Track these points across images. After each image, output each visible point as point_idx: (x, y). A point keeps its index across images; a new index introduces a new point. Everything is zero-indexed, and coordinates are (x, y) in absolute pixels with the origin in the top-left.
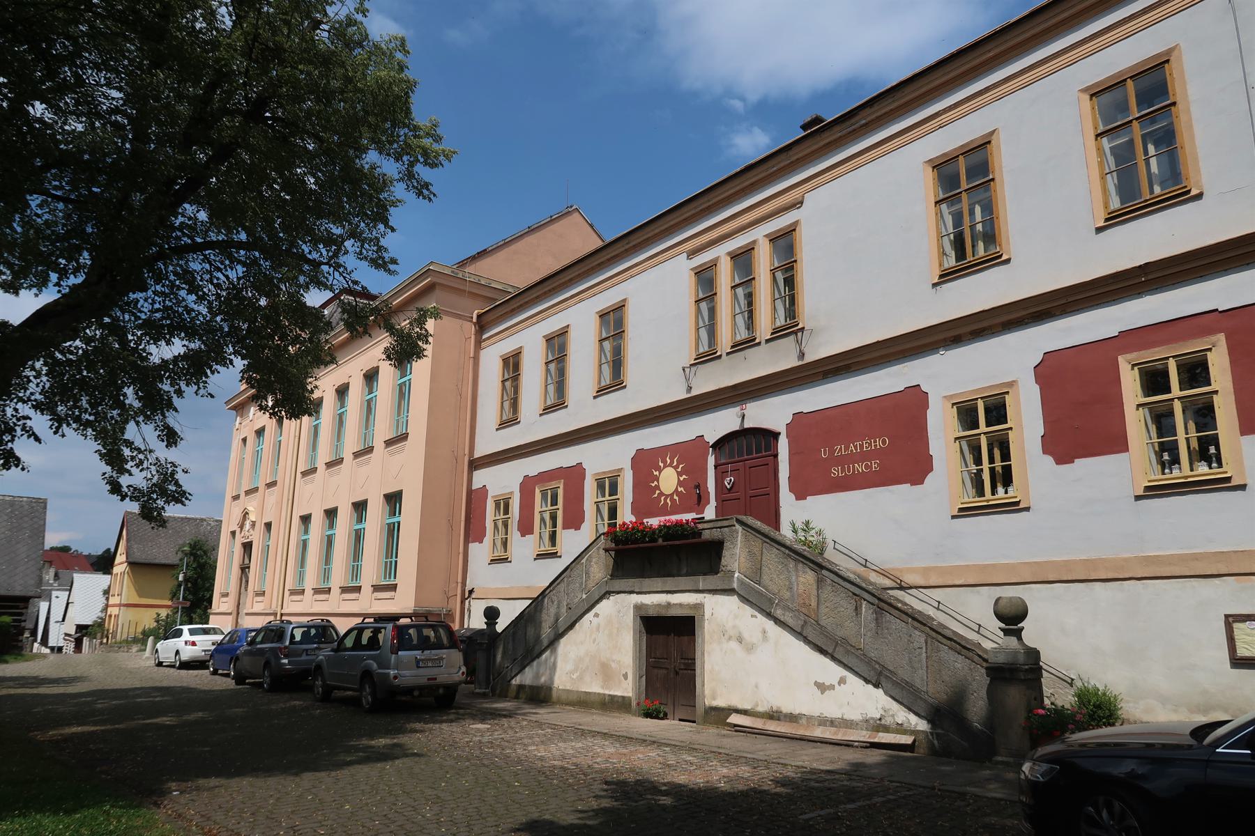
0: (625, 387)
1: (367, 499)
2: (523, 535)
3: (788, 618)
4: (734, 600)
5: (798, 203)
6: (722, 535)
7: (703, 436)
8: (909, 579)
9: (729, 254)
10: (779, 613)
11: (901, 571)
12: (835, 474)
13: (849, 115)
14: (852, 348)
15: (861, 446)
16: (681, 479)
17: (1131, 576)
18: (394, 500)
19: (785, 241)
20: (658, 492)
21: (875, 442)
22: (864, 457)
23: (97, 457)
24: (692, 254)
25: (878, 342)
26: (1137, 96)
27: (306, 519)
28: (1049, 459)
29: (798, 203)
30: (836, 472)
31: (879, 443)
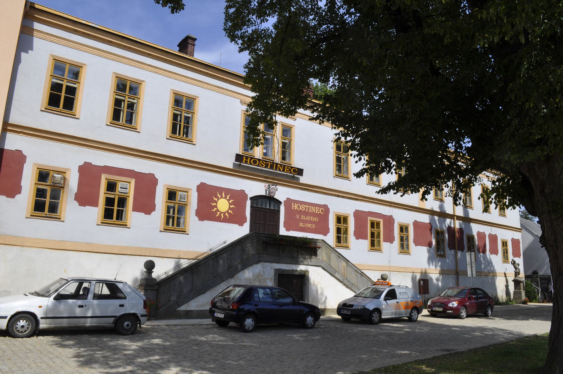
3: (339, 277)
4: (320, 269)
10: (336, 275)
15: (310, 218)
22: (311, 222)
23: (315, 124)
30: (301, 225)
31: (315, 219)
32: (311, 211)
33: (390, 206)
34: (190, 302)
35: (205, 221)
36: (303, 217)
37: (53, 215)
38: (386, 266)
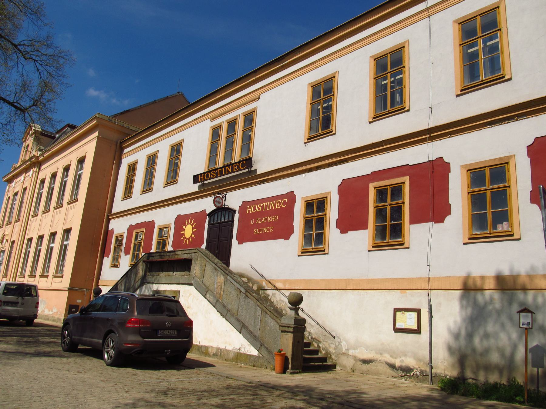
0: (177, 183)
1: (71, 228)
2: (126, 255)
5: (257, 99)
6: (191, 257)
7: (205, 210)
8: (279, 285)
9: (227, 120)
11: (275, 281)
12: (255, 232)
14: (269, 171)
15: (267, 219)
16: (194, 230)
17: (362, 288)
18: (67, 231)
19: (250, 118)
20: (183, 236)
21: (273, 218)
22: (268, 224)
24: (213, 119)
26: (391, 64)
27: (30, 240)
29: (257, 99)
30: (256, 231)
32: (269, 208)
33: (432, 139)
34: (528, 358)
35: (349, 232)
36: (259, 221)
37: (395, 241)
38: (420, 278)
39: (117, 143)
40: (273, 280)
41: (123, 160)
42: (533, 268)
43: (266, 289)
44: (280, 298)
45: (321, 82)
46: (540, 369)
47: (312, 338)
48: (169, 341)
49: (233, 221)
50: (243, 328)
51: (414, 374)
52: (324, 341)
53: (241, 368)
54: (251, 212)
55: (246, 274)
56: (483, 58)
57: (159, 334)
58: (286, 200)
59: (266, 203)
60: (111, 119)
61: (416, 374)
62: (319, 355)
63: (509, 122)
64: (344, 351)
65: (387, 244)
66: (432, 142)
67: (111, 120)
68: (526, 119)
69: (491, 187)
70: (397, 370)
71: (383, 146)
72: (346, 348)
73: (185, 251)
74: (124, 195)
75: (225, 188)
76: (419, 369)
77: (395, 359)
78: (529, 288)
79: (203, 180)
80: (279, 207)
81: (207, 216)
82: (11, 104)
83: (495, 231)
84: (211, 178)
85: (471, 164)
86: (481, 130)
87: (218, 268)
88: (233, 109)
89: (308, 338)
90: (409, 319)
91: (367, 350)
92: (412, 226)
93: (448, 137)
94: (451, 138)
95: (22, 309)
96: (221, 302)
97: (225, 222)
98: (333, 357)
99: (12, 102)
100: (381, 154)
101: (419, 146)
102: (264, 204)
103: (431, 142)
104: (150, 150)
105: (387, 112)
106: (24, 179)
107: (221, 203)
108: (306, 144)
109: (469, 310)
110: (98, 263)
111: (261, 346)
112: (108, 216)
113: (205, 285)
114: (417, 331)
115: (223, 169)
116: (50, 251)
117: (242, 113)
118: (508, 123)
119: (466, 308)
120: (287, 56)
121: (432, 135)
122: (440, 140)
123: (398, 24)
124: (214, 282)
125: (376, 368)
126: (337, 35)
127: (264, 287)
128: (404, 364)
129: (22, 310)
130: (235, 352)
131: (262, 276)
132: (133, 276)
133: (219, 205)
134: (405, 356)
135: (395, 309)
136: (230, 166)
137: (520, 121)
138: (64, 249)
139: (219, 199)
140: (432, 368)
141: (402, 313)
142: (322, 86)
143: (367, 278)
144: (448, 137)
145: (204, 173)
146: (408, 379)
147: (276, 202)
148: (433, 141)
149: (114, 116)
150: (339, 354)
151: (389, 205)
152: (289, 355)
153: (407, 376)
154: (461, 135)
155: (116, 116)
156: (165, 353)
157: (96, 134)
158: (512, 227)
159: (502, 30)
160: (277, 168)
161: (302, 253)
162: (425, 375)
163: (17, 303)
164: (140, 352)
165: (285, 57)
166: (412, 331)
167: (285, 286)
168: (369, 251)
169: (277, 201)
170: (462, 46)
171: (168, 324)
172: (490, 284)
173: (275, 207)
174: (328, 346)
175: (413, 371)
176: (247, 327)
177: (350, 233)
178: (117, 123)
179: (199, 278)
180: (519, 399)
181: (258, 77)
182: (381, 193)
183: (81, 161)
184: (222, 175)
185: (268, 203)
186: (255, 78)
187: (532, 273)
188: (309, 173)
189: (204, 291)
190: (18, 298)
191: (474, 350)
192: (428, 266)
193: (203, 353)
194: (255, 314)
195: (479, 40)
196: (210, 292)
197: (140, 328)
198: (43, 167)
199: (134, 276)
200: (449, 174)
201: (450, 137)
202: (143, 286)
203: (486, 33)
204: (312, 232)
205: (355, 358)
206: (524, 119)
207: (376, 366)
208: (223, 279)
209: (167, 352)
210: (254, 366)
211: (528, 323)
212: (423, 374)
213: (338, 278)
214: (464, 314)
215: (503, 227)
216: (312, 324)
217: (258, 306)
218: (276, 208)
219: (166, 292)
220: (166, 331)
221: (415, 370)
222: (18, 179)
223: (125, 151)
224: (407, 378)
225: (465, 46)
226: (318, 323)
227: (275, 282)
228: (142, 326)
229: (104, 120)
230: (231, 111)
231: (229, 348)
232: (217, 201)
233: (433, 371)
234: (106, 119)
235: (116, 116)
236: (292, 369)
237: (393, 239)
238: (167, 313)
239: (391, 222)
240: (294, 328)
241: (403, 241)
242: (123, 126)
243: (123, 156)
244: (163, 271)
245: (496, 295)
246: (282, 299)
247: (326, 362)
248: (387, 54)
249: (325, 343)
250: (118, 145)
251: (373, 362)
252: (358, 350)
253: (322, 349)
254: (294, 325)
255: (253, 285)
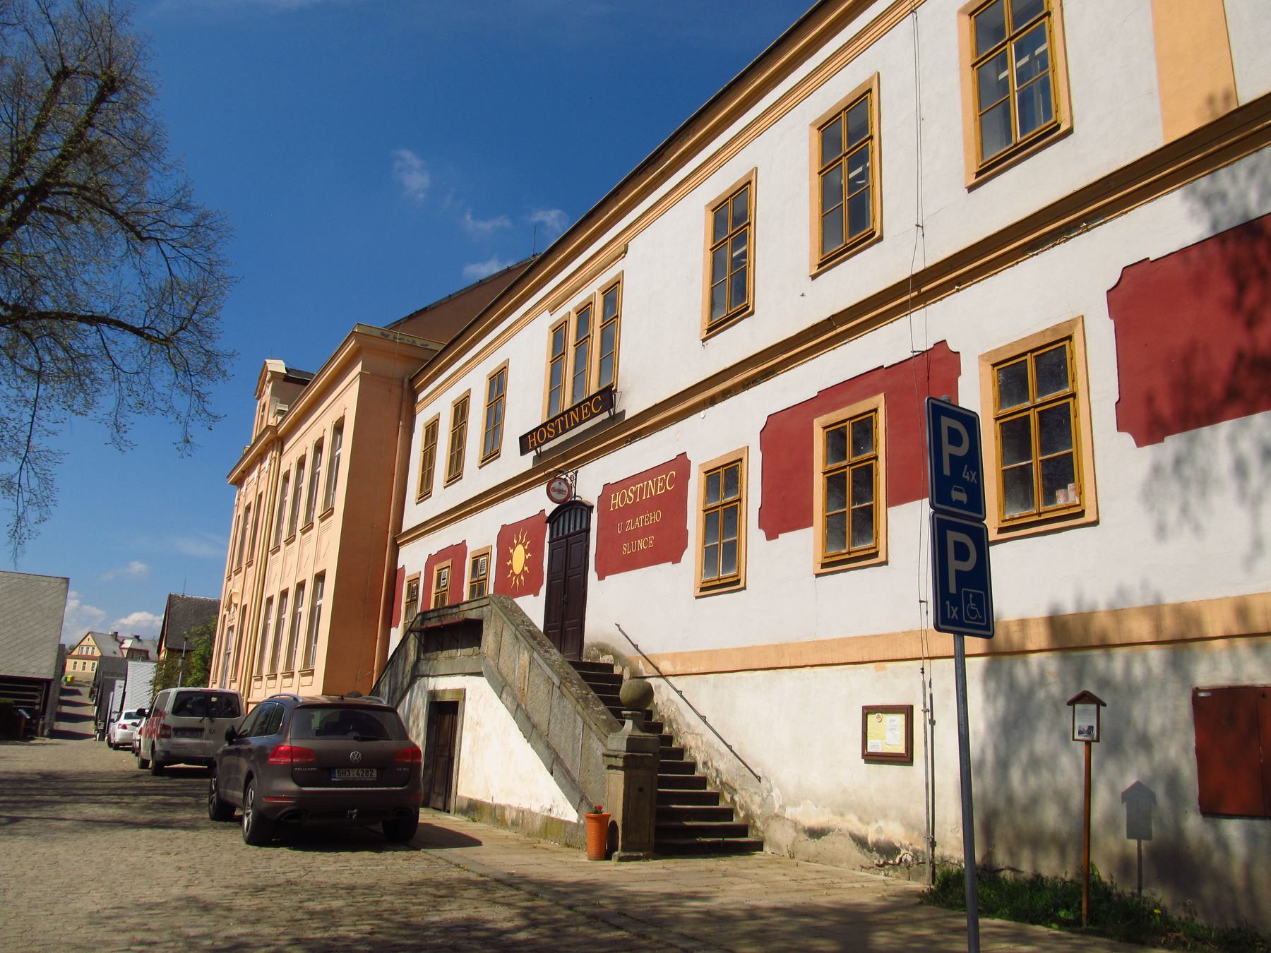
0: (752, 313)
5: (622, 253)
8: (665, 667)
9: (575, 308)
13: (657, 156)
15: (644, 520)
18: (320, 577)
19: (612, 294)
22: (644, 532)
24: (553, 309)
25: (656, 405)
27: (270, 600)
28: (1127, 439)
30: (626, 550)
39: (403, 382)
40: (653, 655)
41: (418, 417)
42: (1122, 593)
43: (644, 675)
44: (668, 696)
45: (727, 199)
46: (1143, 842)
47: (721, 782)
48: (356, 791)
49: (588, 530)
50: (555, 763)
51: (901, 859)
52: (742, 789)
53: (535, 849)
54: (617, 508)
55: (612, 645)
56: (1016, 89)
57: (335, 778)
58: (674, 473)
59: (642, 485)
60: (387, 333)
61: (906, 860)
62: (734, 820)
63: (1071, 238)
64: (776, 810)
65: (847, 556)
66: (926, 306)
67: (387, 336)
68: (1104, 225)
69: (1039, 401)
70: (870, 851)
71: (835, 328)
72: (781, 803)
73: (473, 603)
74: (421, 493)
75: (572, 460)
76: (911, 848)
77: (866, 826)
78: (1118, 642)
79: (535, 445)
80: (663, 491)
81: (547, 522)
82: (138, 332)
83: (1051, 507)
84: (548, 440)
85: (997, 349)
86: (1017, 263)
87: (519, 636)
88: (584, 283)
89: (716, 783)
90: (890, 730)
91: (816, 807)
92: (892, 510)
93: (955, 290)
94: (961, 292)
95: (212, 742)
96: (524, 707)
97: (576, 533)
98: (758, 824)
99: (141, 328)
100: (834, 349)
101: (903, 318)
102: (639, 486)
103: (923, 307)
104: (455, 393)
105: (843, 247)
106: (259, 477)
107: (565, 491)
108: (705, 343)
109: (1001, 703)
110: (380, 641)
111: (582, 800)
112: (394, 540)
113: (501, 674)
114: (906, 759)
115: (566, 416)
116: (296, 617)
117: (599, 289)
118: (1068, 239)
119: (995, 697)
120: (667, 149)
121: (923, 290)
122: (941, 299)
123: (858, 39)
124: (515, 667)
125: (832, 846)
126: (750, 86)
127: (641, 671)
128: (882, 838)
129: (210, 744)
130: (543, 816)
131: (636, 647)
132: (401, 662)
133: (561, 497)
134: (885, 816)
135: (864, 708)
136: (577, 409)
137: (1094, 229)
138: (315, 612)
139: (560, 484)
140: (933, 844)
141: (878, 717)
142: (730, 206)
143: (815, 639)
144: (955, 290)
145: (544, 425)
146: (891, 873)
147: (657, 480)
148: (928, 303)
149: (392, 326)
150: (767, 819)
151: (850, 465)
152: (618, 817)
153: (888, 864)
154: (979, 281)
155: (399, 325)
156: (348, 817)
157: (358, 369)
158: (1081, 493)
159: (1052, 16)
160: (653, 404)
161: (702, 589)
162: (921, 863)
163: (202, 730)
164: (293, 814)
165: (665, 151)
166: (895, 759)
167: (674, 667)
168: (816, 577)
169: (659, 478)
170: (978, 69)
171: (354, 755)
172: (1038, 637)
173: (656, 492)
174: (748, 801)
175: (899, 853)
176: (562, 760)
177: (783, 537)
178: (399, 339)
179: (494, 660)
180: (1065, 915)
181: (621, 203)
182: (836, 436)
183: (339, 428)
184: (565, 431)
185: (645, 483)
186: (617, 207)
187: (1118, 607)
188: (711, 409)
189: (501, 686)
190: (202, 720)
191: (1010, 800)
192: (921, 601)
193: (498, 820)
194: (573, 731)
195: (1007, 46)
196: (508, 687)
197: (292, 765)
198: (286, 447)
199: (403, 664)
200: (959, 378)
201: (958, 291)
202: (415, 682)
203: (1021, 28)
204: (735, 538)
205: (795, 824)
206: (1101, 224)
207: (833, 843)
208: (528, 658)
209: (351, 815)
210: (568, 845)
211: (1091, 728)
212: (917, 860)
213: (765, 643)
214: (991, 712)
215: (1064, 498)
216: (722, 752)
217: (579, 714)
218: (659, 493)
219: (447, 694)
220: (351, 770)
221: (903, 851)
222: (250, 478)
223: (421, 396)
224: (888, 870)
225: (990, 63)
226: (730, 747)
227: (658, 659)
228: (298, 760)
229: (372, 336)
230: (582, 286)
231: (536, 808)
232: (556, 488)
233: (938, 851)
234: (375, 335)
235: (397, 325)
236: (624, 849)
237: (859, 544)
238: (355, 734)
239: (854, 505)
240: (625, 758)
241: (875, 548)
242: (413, 346)
243: (418, 409)
244: (442, 649)
245: (1050, 663)
246: (671, 697)
247: (746, 836)
248: (840, 113)
249: (743, 793)
250: (406, 385)
251: (827, 834)
252: (802, 806)
253: (738, 807)
254: (627, 751)
255: (623, 670)
